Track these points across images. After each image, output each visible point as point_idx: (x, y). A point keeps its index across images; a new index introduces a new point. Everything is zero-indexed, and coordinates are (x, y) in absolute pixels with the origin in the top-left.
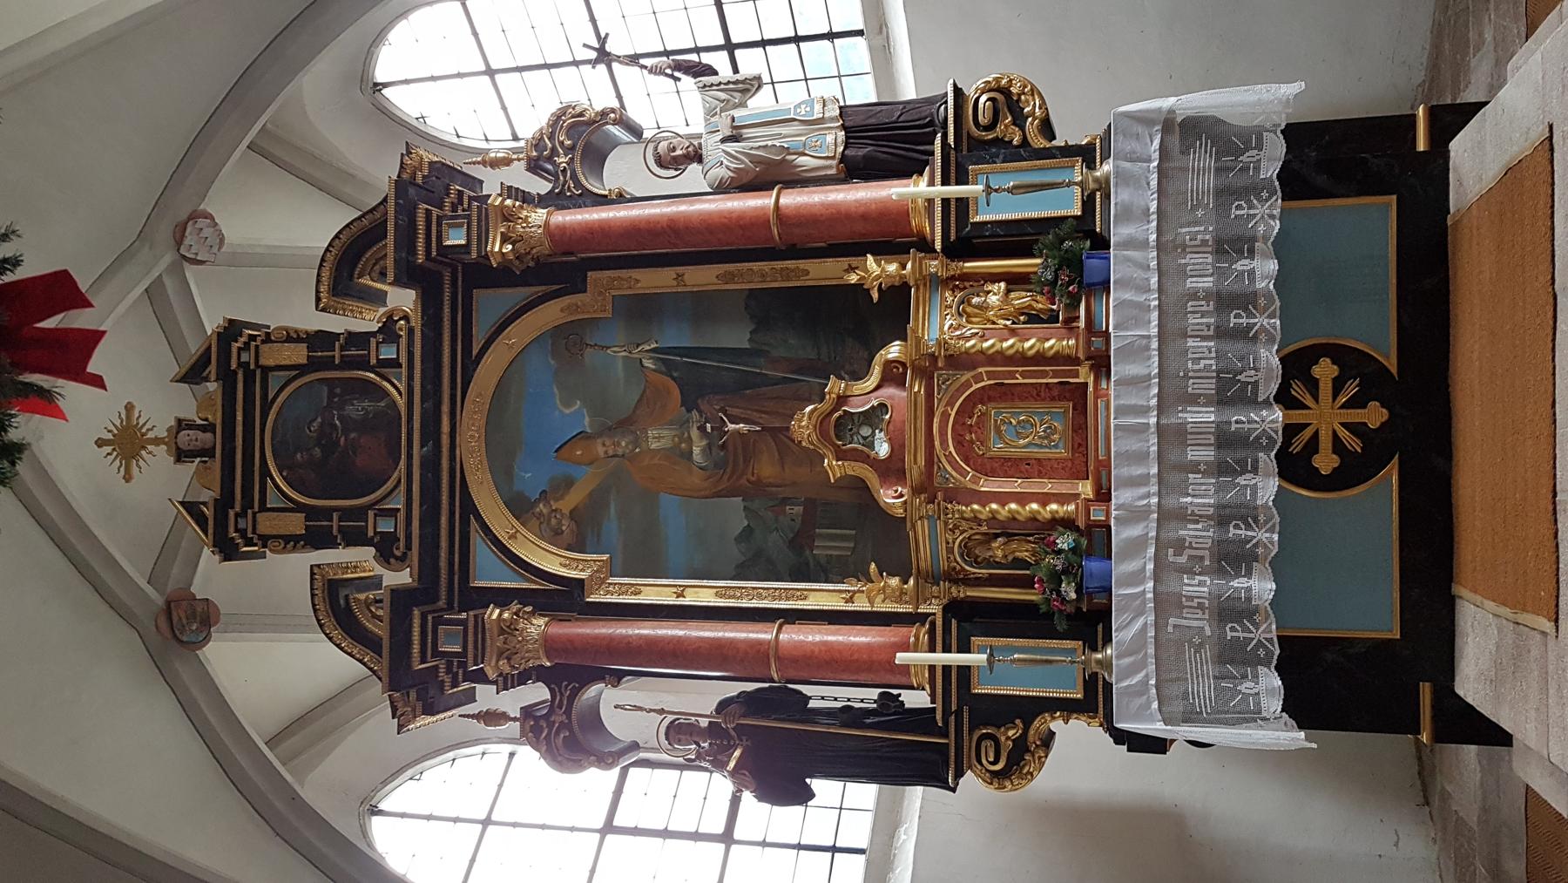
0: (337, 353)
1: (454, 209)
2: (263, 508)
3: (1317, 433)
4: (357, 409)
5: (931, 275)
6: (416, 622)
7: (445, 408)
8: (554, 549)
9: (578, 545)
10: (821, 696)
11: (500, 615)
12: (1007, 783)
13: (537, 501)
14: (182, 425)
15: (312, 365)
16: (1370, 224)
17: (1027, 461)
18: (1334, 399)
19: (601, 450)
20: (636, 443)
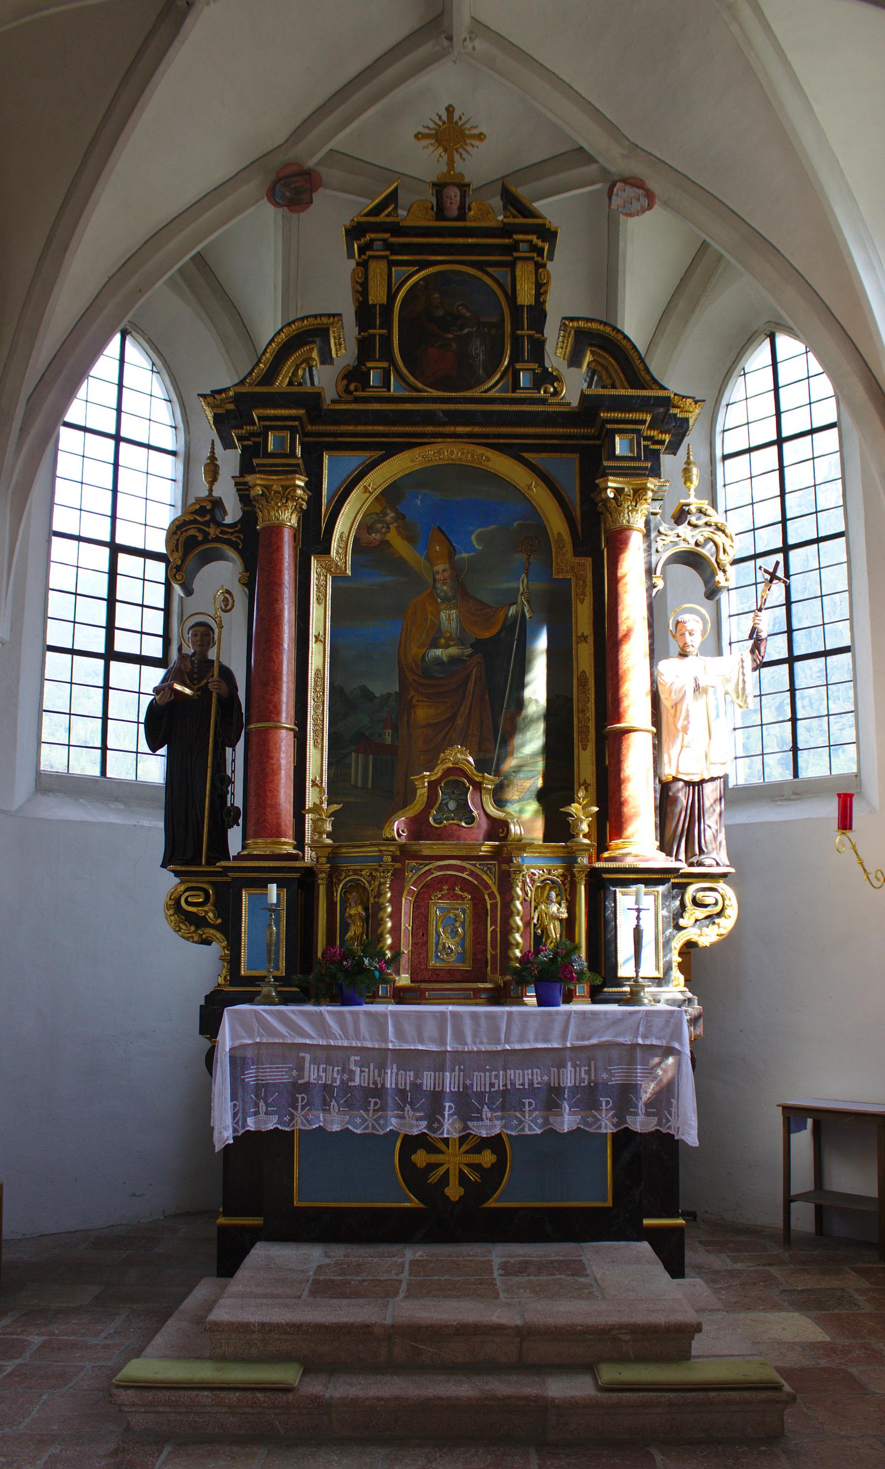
0: (525, 332)
1: (646, 438)
2: (391, 264)
3: (442, 1152)
4: (478, 350)
5: (576, 858)
6: (293, 412)
7: (477, 430)
8: (355, 526)
9: (359, 547)
10: (236, 757)
11: (299, 487)
12: (171, 912)
14: (463, 187)
15: (516, 310)
16: (598, 1192)
17: (426, 933)
18: (466, 1164)
19: (439, 568)
20: (446, 599)
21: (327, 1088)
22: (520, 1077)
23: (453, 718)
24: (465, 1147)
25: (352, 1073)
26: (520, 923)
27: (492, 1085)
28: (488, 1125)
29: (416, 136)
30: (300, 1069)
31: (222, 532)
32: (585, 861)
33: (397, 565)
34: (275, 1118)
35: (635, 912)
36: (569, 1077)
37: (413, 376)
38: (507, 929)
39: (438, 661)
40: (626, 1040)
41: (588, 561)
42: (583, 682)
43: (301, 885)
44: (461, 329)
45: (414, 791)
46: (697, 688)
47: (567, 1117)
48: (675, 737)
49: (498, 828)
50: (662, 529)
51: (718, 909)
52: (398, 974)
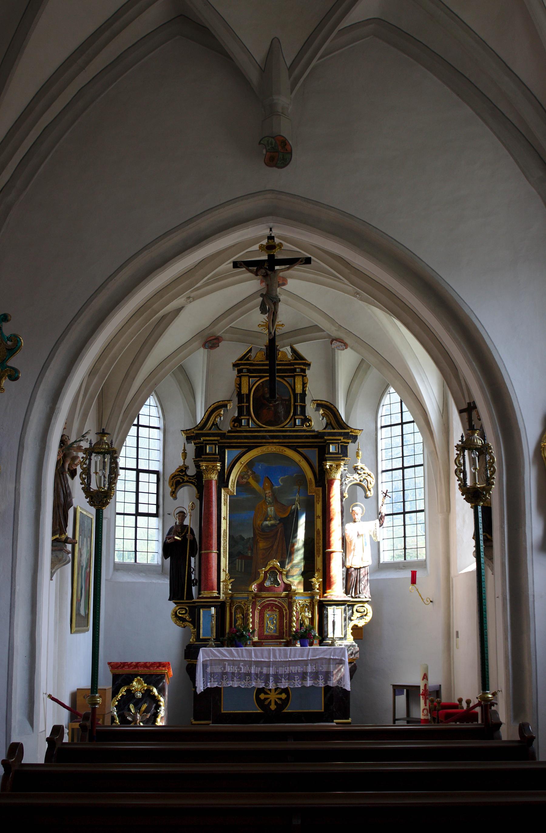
2: (250, 377)
6: (216, 438)
13: (252, 470)
17: (263, 623)
19: (267, 492)
20: (270, 503)
21: (233, 673)
22: (294, 669)
23: (272, 547)
24: (277, 693)
25: (241, 668)
26: (295, 619)
27: (285, 672)
28: (284, 685)
29: (258, 326)
30: (225, 668)
31: (189, 479)
32: (318, 598)
33: (252, 491)
34: (217, 683)
35: (335, 615)
36: (309, 670)
37: (258, 421)
38: (291, 621)
39: (267, 526)
40: (328, 657)
41: (320, 489)
42: (318, 533)
43: (221, 607)
44: (275, 402)
45: (259, 574)
46: (358, 535)
47: (309, 682)
48: (351, 552)
49: (288, 587)
50: (348, 476)
51: (365, 613)
52: (254, 637)
